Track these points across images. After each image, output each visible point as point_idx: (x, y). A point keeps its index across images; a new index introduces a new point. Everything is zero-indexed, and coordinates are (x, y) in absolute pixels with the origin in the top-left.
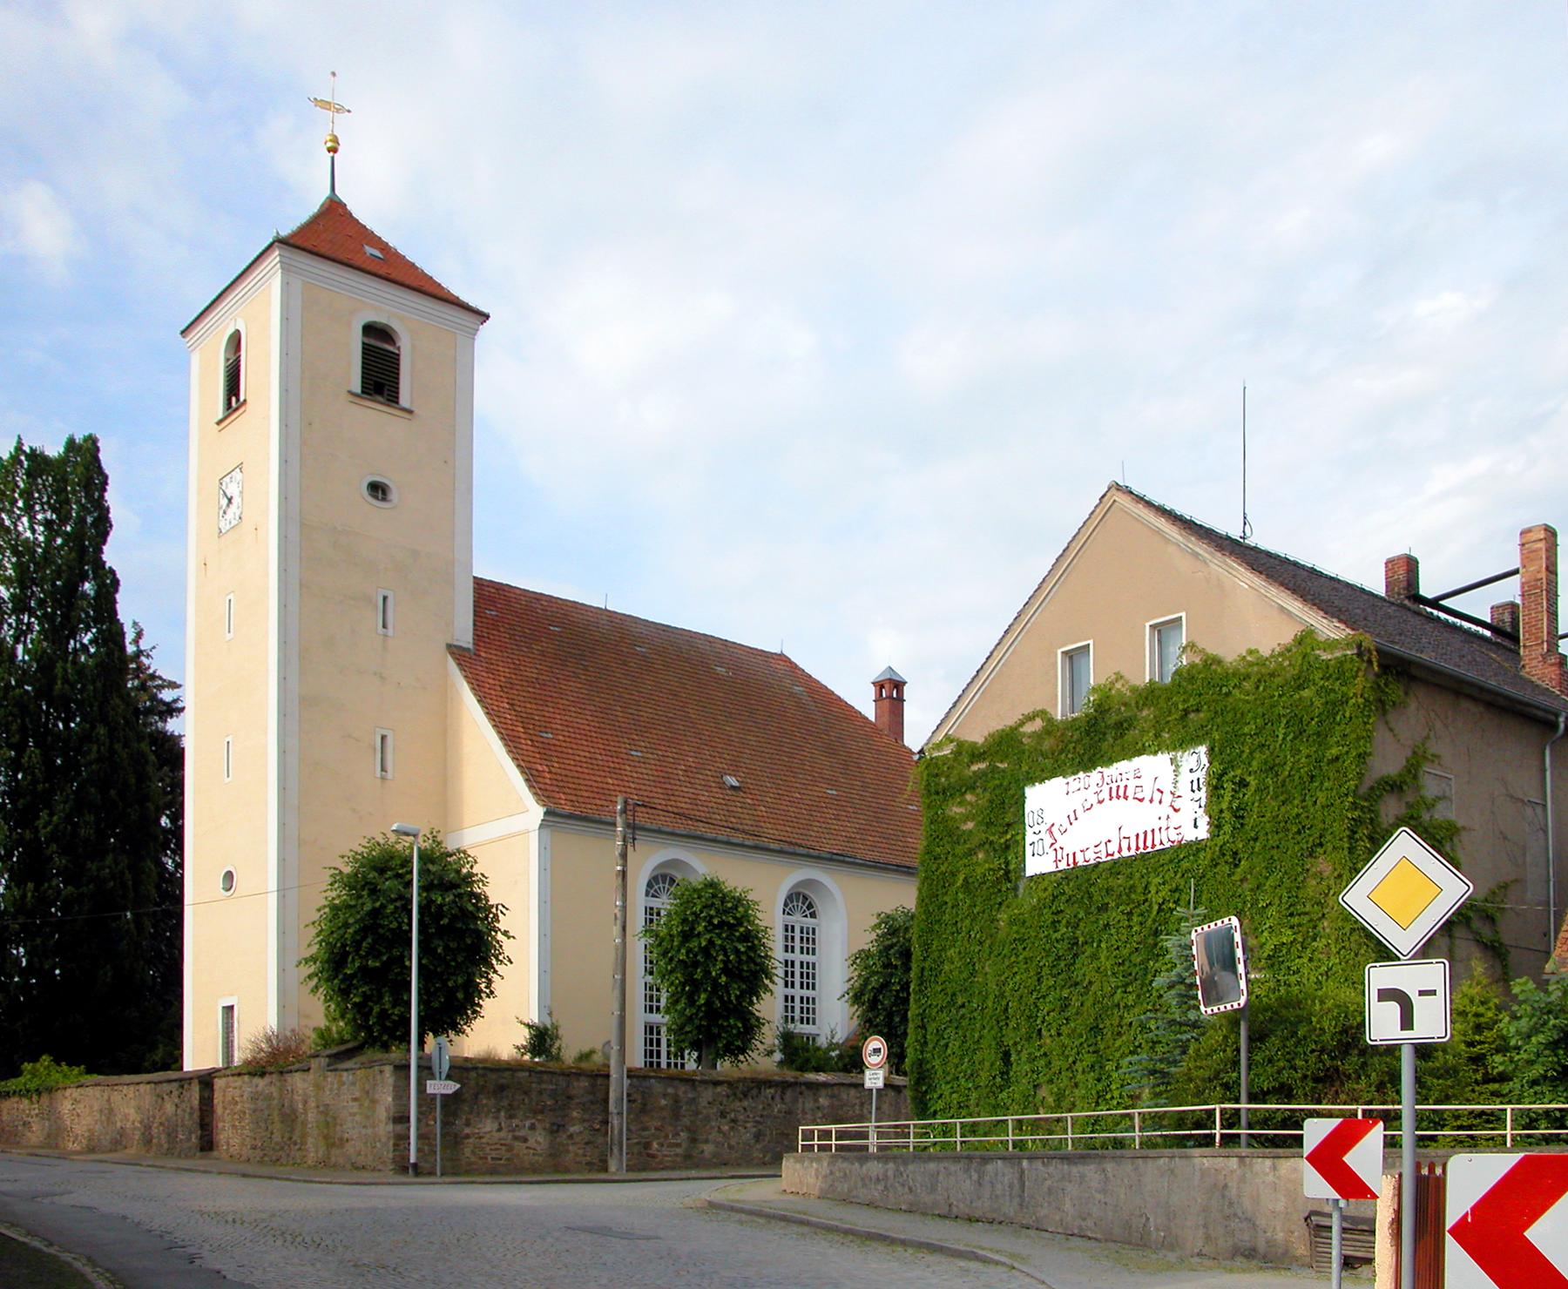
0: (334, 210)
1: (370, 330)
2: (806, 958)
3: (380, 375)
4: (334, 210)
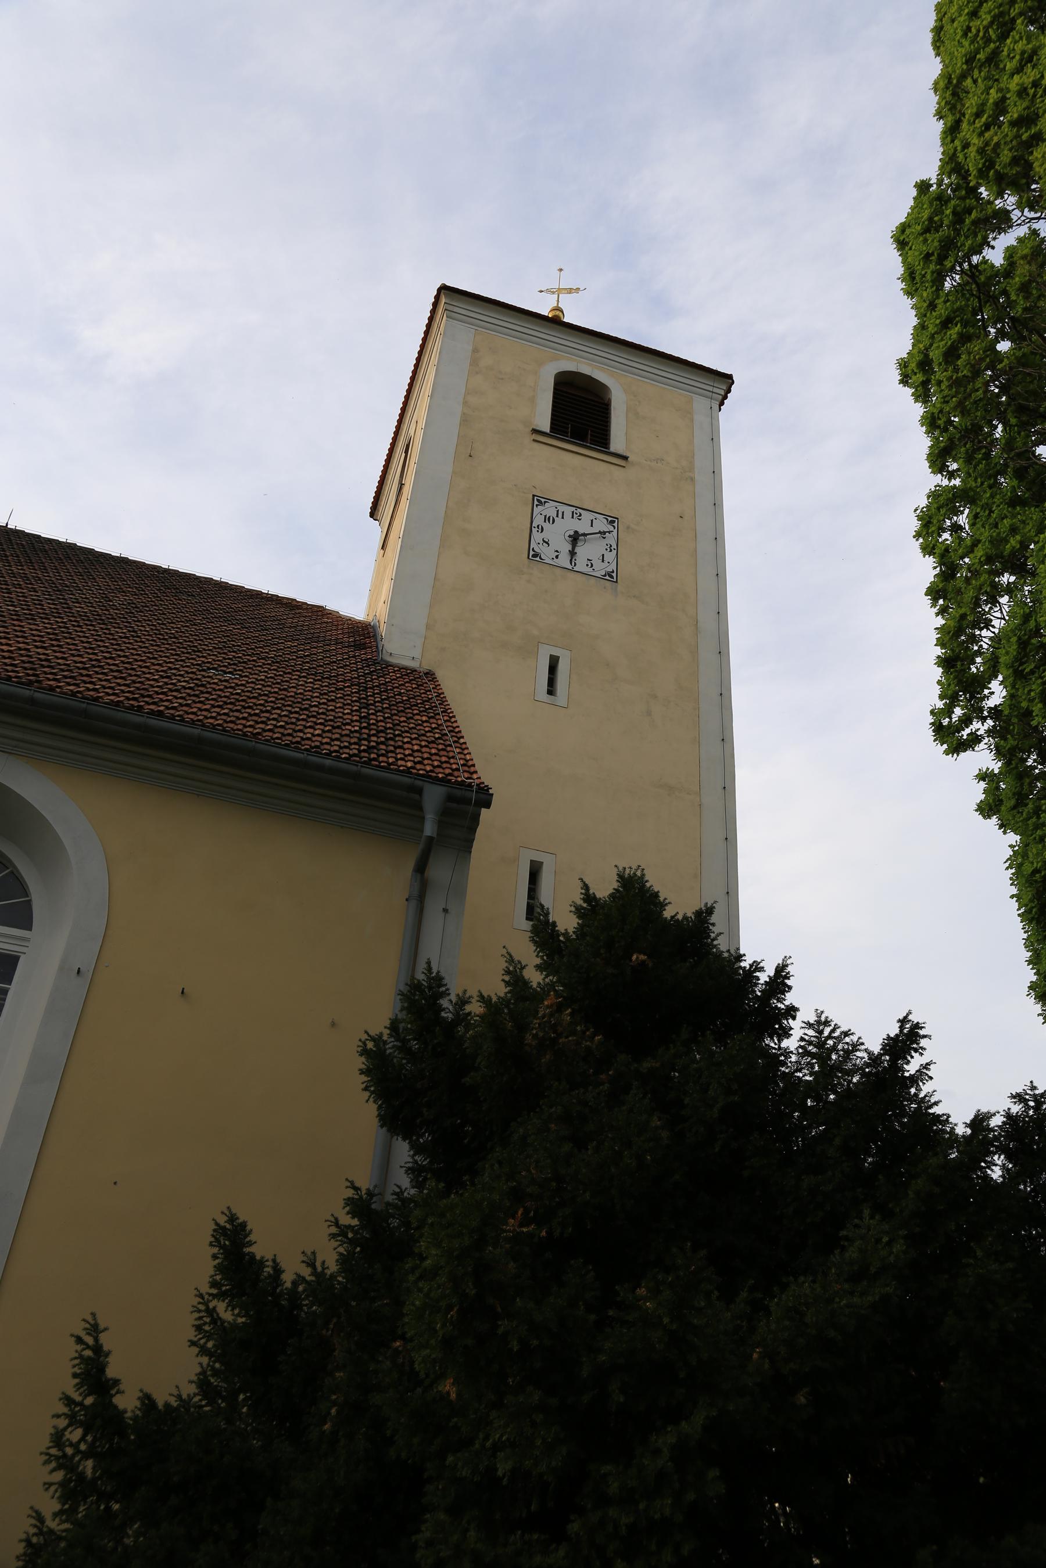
3: (581, 414)
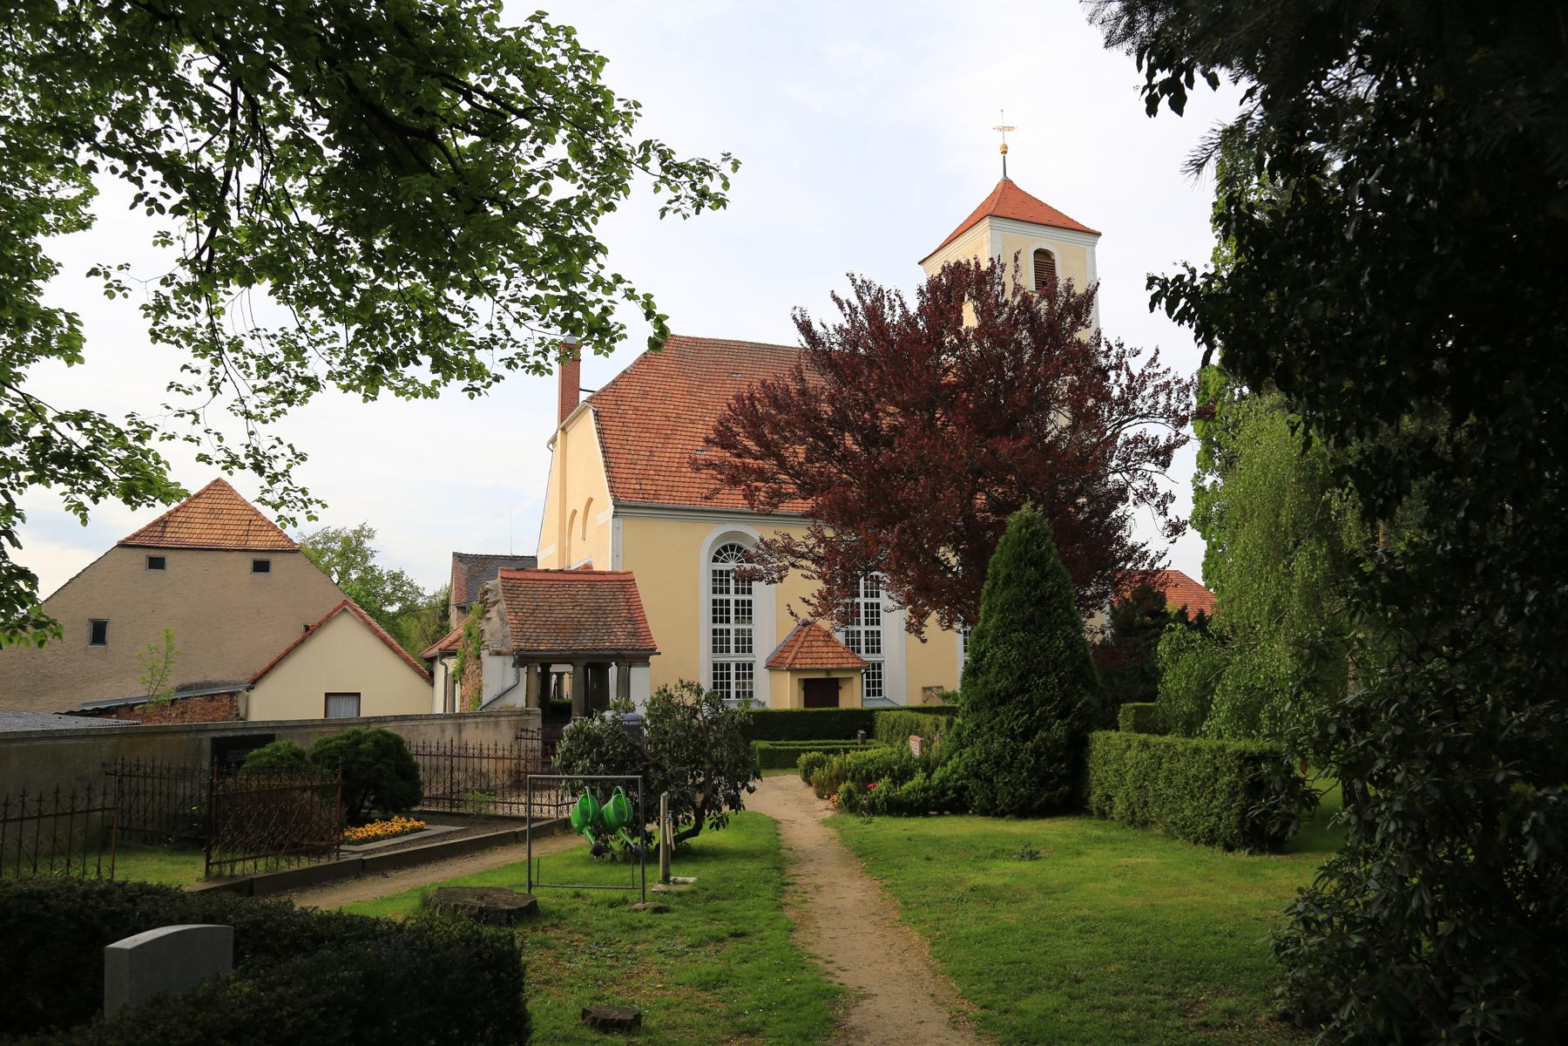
0: (1007, 186)
1: (1039, 253)
2: (722, 658)
4: (1007, 186)
